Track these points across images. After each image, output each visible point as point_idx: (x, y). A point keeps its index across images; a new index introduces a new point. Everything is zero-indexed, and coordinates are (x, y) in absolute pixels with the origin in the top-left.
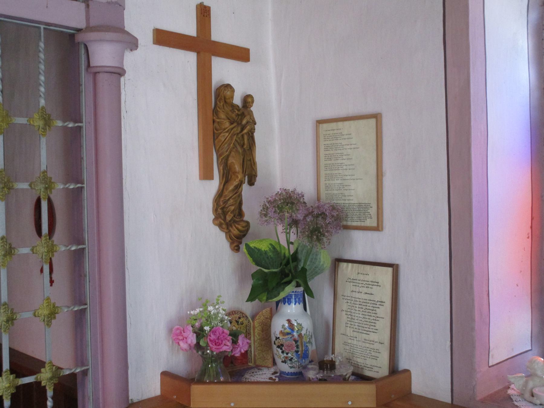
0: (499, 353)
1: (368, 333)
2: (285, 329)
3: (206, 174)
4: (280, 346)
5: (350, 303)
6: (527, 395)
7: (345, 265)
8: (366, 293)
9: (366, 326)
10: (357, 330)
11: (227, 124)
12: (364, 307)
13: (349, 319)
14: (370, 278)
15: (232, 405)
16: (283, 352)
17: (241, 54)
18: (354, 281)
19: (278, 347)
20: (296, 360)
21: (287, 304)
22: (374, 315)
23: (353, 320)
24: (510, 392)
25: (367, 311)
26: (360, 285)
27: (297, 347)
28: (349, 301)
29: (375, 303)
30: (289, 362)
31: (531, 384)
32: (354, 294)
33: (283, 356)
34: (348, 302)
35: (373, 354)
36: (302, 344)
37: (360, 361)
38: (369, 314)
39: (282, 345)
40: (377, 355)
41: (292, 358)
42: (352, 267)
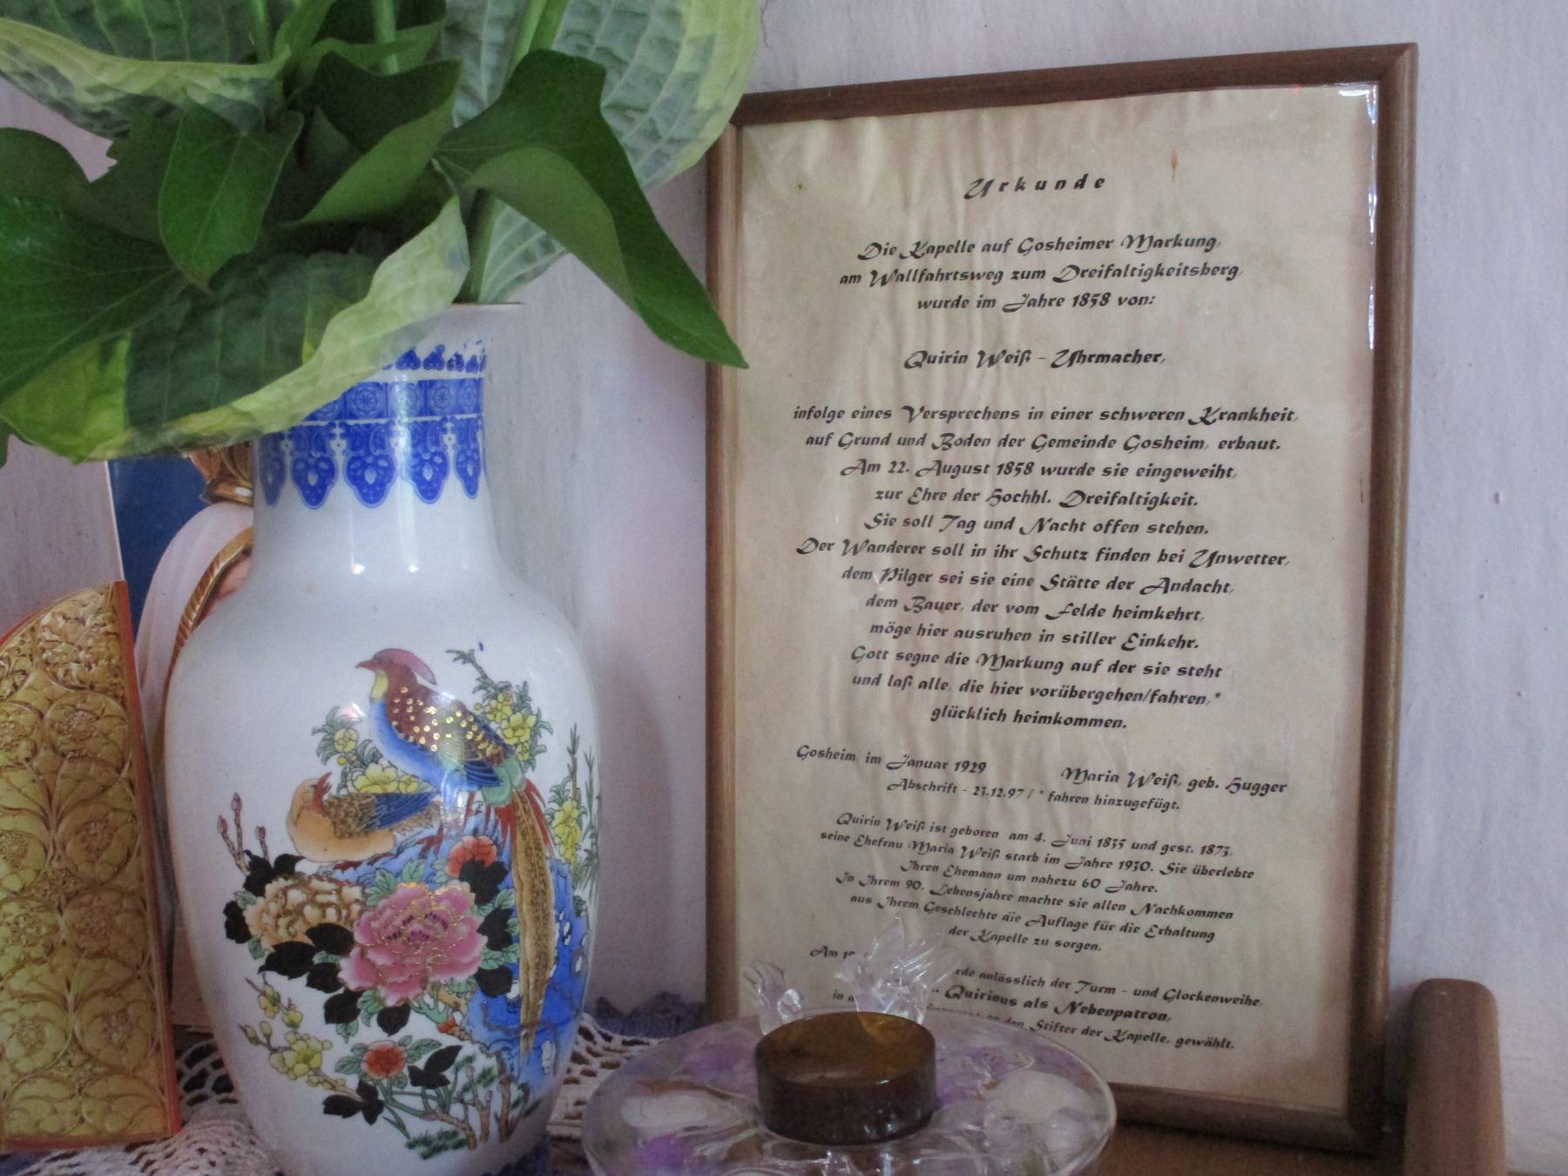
1: (1108, 709)
2: (362, 760)
5: (897, 467)
8: (1078, 357)
9: (1087, 653)
10: (985, 700)
12: (1059, 488)
13: (886, 616)
16: (341, 1011)
18: (935, 264)
19: (287, 960)
20: (483, 1062)
21: (342, 492)
22: (1173, 543)
23: (934, 618)
25: (1093, 514)
26: (1009, 292)
27: (498, 931)
28: (881, 455)
29: (1178, 430)
30: (411, 1097)
32: (936, 386)
33: (336, 1047)
34: (866, 467)
35: (1169, 890)
36: (538, 895)
38: (1121, 542)
39: (334, 938)
40: (1216, 892)
41: (446, 1057)
42: (901, 156)
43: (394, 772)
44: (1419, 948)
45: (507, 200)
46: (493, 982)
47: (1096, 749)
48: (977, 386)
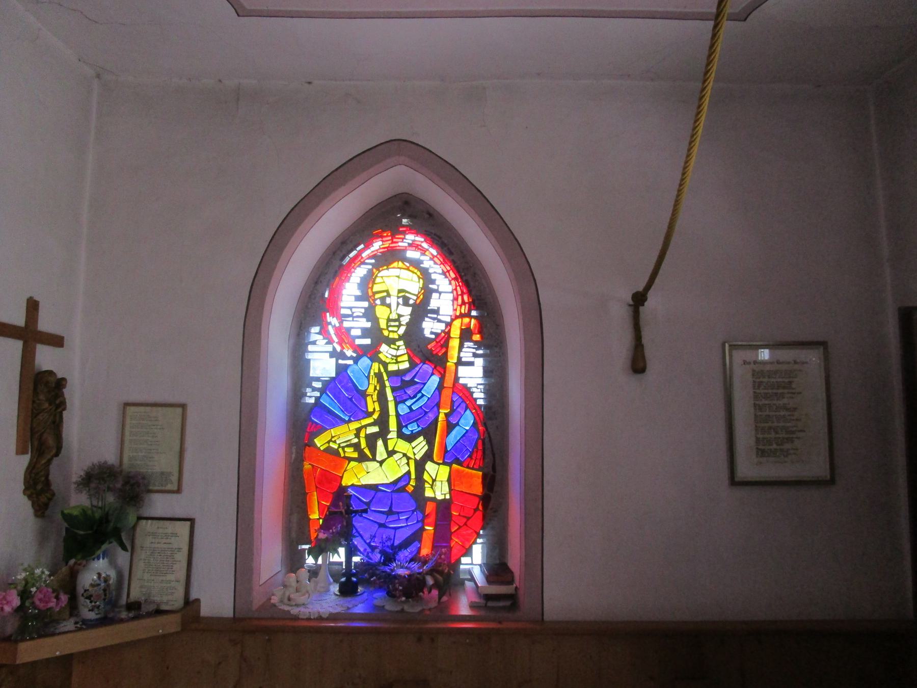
0: (264, 576)
3: (21, 451)
4: (89, 597)
6: (286, 601)
7: (144, 522)
11: (46, 405)
14: (169, 531)
15: (58, 653)
17: (57, 341)
19: (87, 598)
24: (272, 601)
27: (105, 595)
31: (287, 594)
32: (153, 545)
33: (90, 605)
37: (157, 599)
43: (98, 582)
44: (194, 595)
45: (177, 633)
46: (104, 599)
47: (164, 578)
48: (156, 546)
